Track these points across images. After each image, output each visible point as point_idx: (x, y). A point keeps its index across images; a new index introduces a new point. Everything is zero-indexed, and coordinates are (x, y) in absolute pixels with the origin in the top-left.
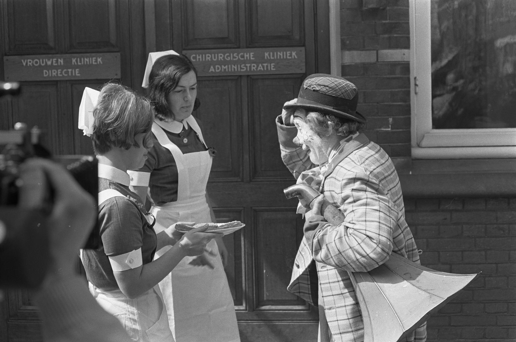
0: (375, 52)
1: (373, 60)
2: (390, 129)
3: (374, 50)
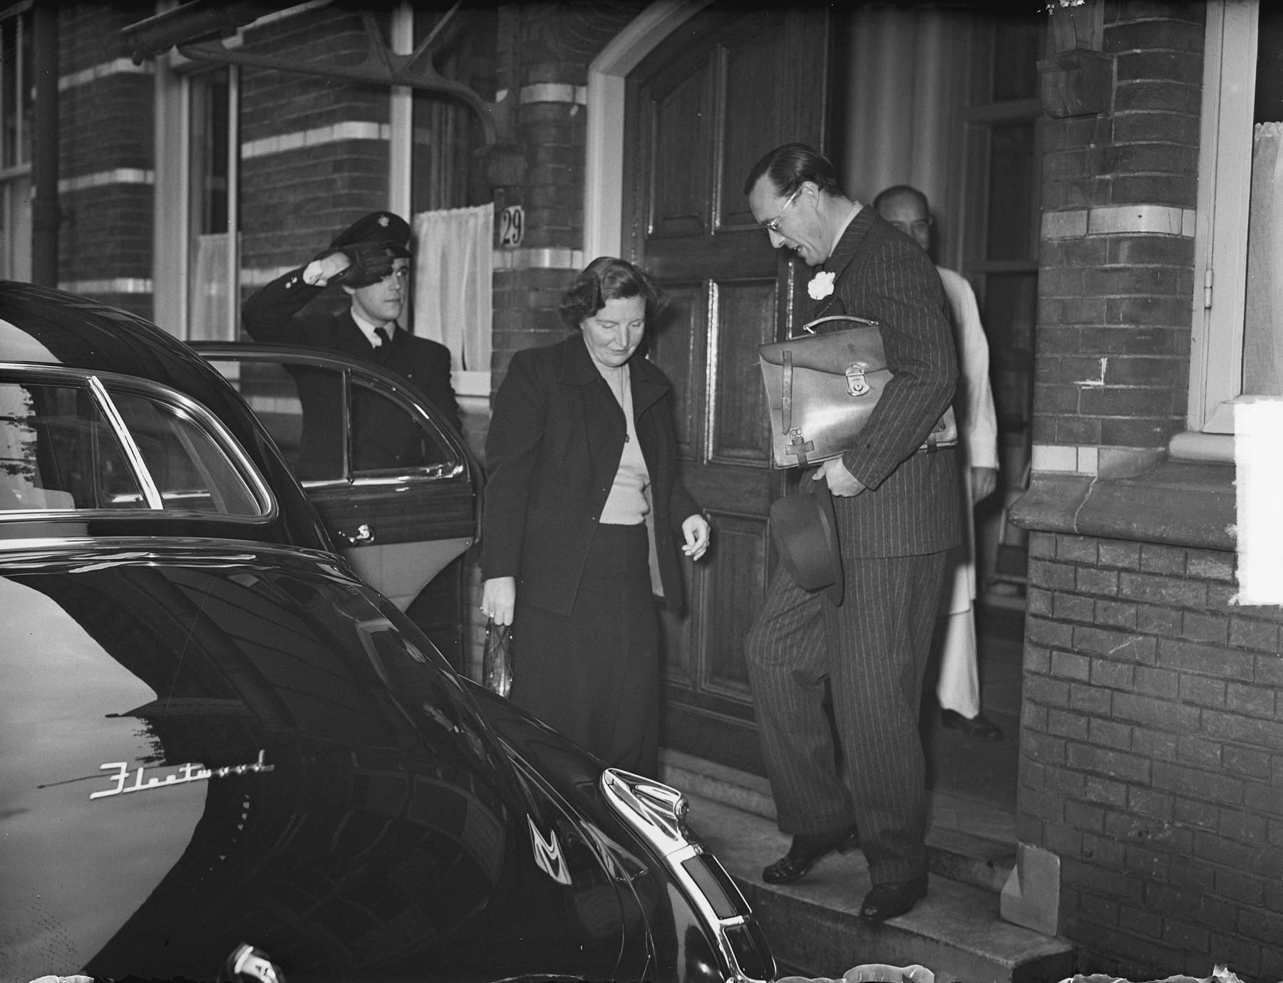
0: (1085, 212)
1: (1080, 230)
2: (1101, 383)
3: (1083, 209)
